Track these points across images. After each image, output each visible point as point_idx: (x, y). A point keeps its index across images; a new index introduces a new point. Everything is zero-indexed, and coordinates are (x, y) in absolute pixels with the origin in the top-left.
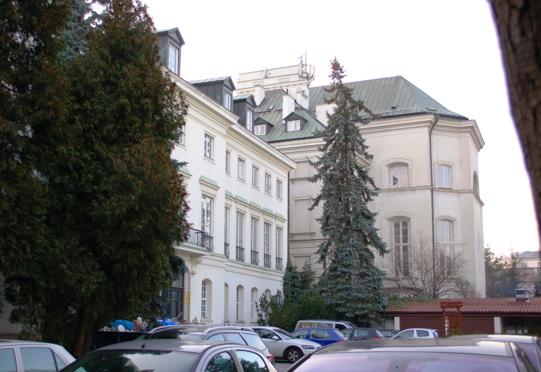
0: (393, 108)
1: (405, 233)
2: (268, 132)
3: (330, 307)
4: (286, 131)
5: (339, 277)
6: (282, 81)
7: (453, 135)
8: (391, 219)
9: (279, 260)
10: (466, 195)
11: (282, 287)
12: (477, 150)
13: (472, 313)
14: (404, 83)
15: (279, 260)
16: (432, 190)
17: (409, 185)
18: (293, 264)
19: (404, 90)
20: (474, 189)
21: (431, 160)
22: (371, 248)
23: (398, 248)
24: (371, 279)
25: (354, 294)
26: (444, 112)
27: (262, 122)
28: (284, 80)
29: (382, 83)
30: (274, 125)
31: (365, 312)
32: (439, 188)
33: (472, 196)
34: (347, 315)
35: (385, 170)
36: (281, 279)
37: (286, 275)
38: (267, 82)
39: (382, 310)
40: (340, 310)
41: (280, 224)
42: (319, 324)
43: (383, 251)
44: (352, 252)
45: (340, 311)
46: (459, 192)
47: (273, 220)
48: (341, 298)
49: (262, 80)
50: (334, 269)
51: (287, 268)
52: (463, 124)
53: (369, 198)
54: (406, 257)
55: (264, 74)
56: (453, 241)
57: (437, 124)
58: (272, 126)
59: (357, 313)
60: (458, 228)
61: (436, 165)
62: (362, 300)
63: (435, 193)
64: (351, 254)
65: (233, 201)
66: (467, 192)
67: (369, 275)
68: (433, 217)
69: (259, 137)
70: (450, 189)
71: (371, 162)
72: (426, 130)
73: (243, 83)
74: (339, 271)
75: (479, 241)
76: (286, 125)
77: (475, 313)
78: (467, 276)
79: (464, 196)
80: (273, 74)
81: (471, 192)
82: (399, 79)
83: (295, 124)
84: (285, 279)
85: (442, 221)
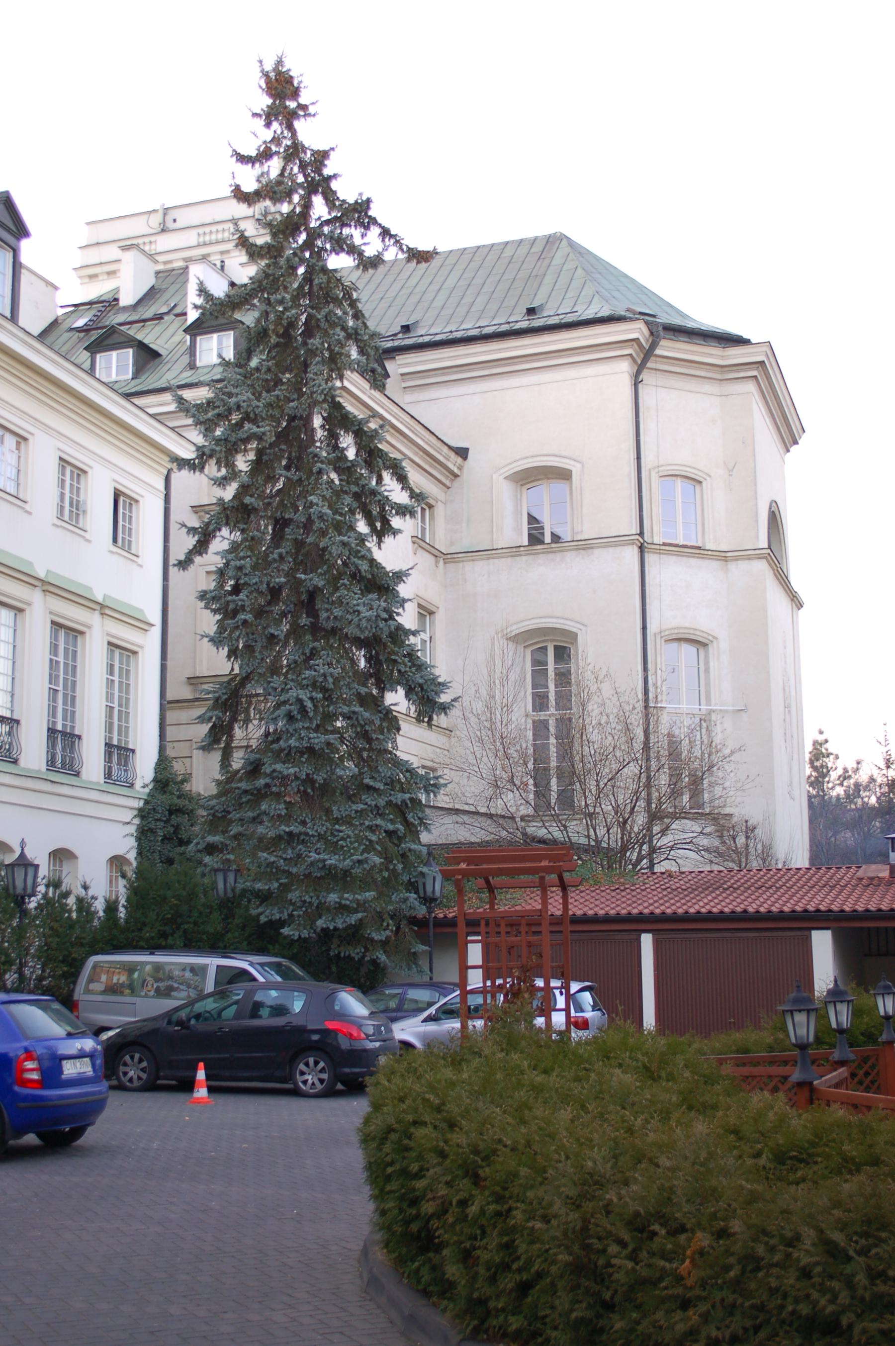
0: (531, 311)
1: (563, 678)
2: (138, 372)
3: (229, 905)
4: (192, 366)
5: (265, 796)
6: (207, 238)
7: (707, 387)
8: (520, 638)
9: (118, 753)
10: (743, 565)
11: (132, 842)
12: (782, 449)
13: (733, 917)
14: (568, 250)
15: (118, 753)
16: (642, 548)
17: (573, 533)
18: (178, 767)
19: (569, 266)
20: (769, 548)
21: (639, 458)
22: (397, 699)
23: (540, 727)
24: (382, 802)
25: (314, 856)
26: (677, 321)
27: (122, 339)
28: (214, 237)
29: (508, 252)
30: (161, 351)
31: (353, 919)
32: (664, 544)
33: (762, 567)
34: (285, 931)
35: (505, 491)
36: (128, 816)
37: (147, 802)
38: (164, 243)
39: (421, 911)
40: (267, 913)
41: (127, 635)
42: (158, 967)
43: (428, 701)
44: (309, 704)
45: (263, 919)
46: (724, 557)
47: (94, 619)
48: (271, 871)
49: (153, 239)
50: (254, 769)
51: (155, 780)
52: (736, 355)
53: (386, 522)
54: (566, 753)
55: (155, 221)
56: (708, 702)
57: (658, 352)
58: (156, 355)
59: (320, 923)
60: (721, 662)
61: (654, 475)
62: (341, 878)
63: (650, 558)
64: (303, 710)
65: (97, 613)
66: (749, 558)
67: (376, 790)
68: (644, 628)
69: (109, 386)
70: (699, 548)
71: (460, 468)
72: (624, 368)
73: (96, 249)
74: (266, 775)
75: (787, 707)
76: (192, 350)
77: (745, 917)
78: (742, 806)
79: (740, 569)
80: (185, 218)
81: (760, 557)
82: (554, 241)
83: (220, 342)
84: (142, 814)
85: (675, 645)
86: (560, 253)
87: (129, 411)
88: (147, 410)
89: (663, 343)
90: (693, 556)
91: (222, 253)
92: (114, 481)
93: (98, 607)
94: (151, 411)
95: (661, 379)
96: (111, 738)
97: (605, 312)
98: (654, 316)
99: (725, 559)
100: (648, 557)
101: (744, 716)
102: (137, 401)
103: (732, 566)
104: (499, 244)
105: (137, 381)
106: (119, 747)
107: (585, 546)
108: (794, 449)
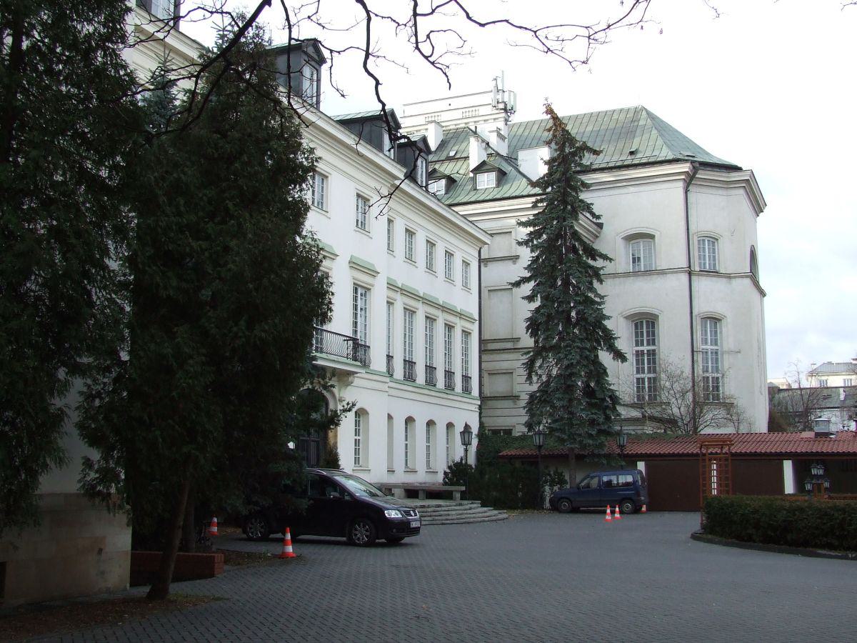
0: (632, 153)
7: (720, 192)
10: (739, 280)
12: (754, 214)
16: (690, 274)
21: (688, 229)
29: (615, 116)
33: (748, 281)
35: (620, 244)
41: (468, 325)
52: (735, 176)
57: (697, 176)
65: (458, 318)
66: (742, 277)
68: (691, 313)
71: (599, 233)
72: (681, 184)
75: (759, 348)
81: (747, 277)
87: (431, 200)
89: (700, 172)
90: (714, 276)
91: (475, 122)
92: (427, 236)
93: (399, 290)
94: (461, 213)
95: (699, 189)
96: (405, 357)
97: (670, 157)
98: (694, 157)
99: (730, 278)
100: (693, 277)
101: (739, 355)
102: (453, 208)
104: (610, 111)
106: (409, 362)
107: (662, 272)
108: (761, 214)
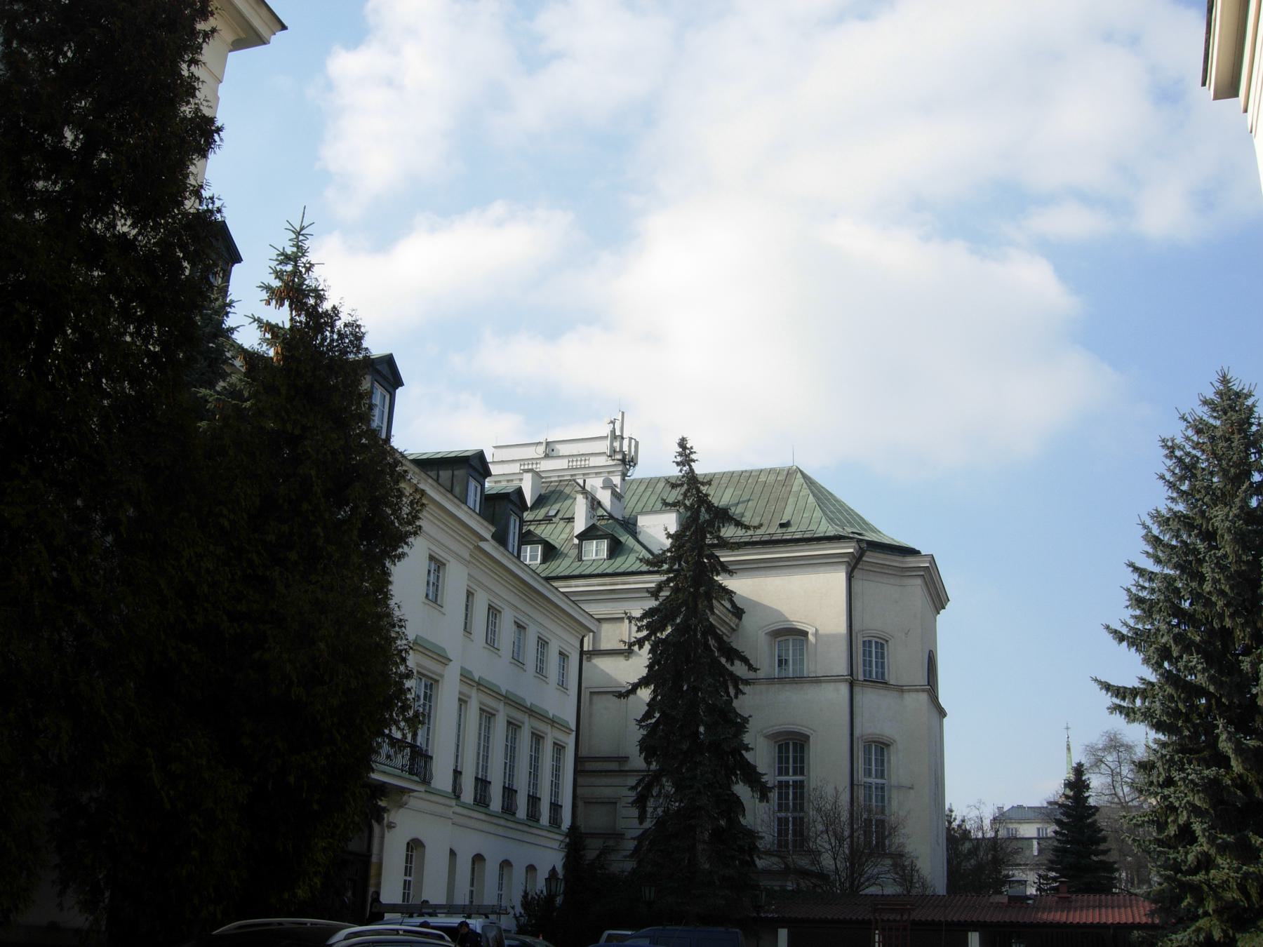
0: (782, 525)
4: (580, 559)
10: (913, 695)
15: (556, 808)
16: (851, 685)
36: (556, 845)
41: (562, 737)
68: (852, 734)
80: (563, 449)
81: (923, 691)
86: (796, 483)
88: (583, 606)
89: (868, 553)
103: (906, 695)
105: (544, 566)
107: (817, 680)
